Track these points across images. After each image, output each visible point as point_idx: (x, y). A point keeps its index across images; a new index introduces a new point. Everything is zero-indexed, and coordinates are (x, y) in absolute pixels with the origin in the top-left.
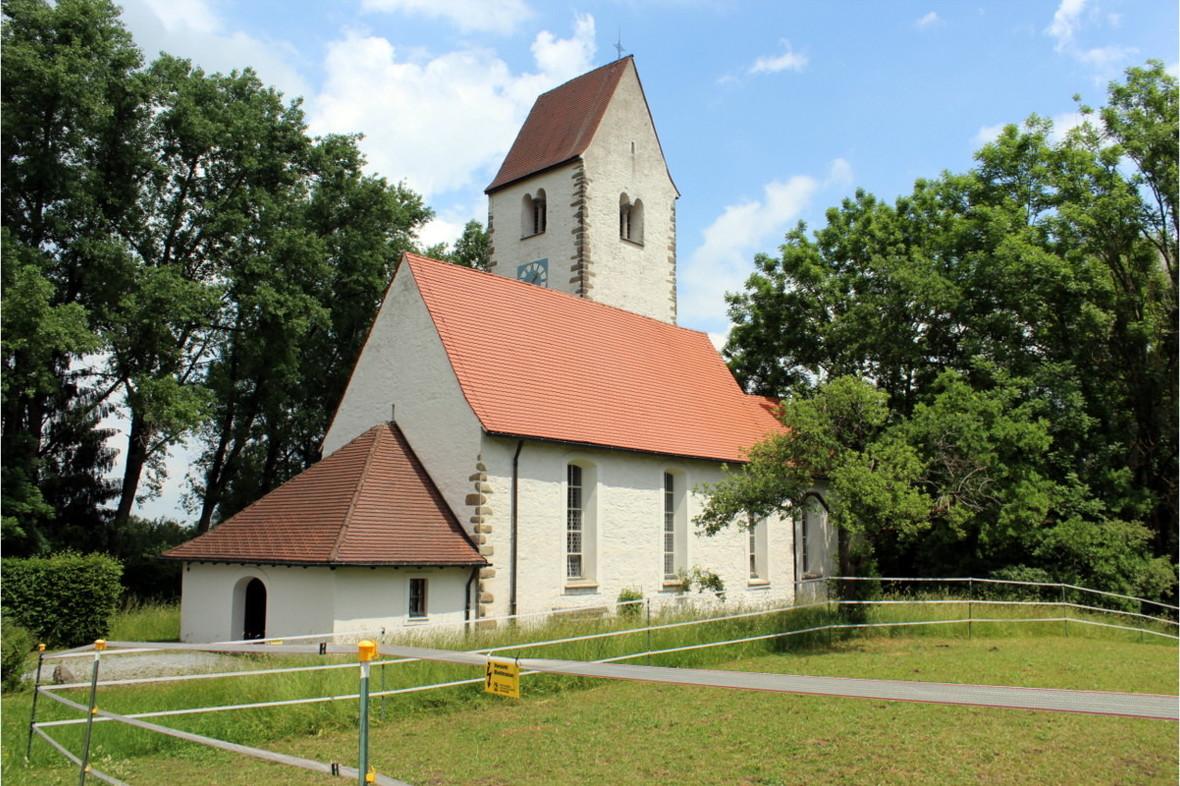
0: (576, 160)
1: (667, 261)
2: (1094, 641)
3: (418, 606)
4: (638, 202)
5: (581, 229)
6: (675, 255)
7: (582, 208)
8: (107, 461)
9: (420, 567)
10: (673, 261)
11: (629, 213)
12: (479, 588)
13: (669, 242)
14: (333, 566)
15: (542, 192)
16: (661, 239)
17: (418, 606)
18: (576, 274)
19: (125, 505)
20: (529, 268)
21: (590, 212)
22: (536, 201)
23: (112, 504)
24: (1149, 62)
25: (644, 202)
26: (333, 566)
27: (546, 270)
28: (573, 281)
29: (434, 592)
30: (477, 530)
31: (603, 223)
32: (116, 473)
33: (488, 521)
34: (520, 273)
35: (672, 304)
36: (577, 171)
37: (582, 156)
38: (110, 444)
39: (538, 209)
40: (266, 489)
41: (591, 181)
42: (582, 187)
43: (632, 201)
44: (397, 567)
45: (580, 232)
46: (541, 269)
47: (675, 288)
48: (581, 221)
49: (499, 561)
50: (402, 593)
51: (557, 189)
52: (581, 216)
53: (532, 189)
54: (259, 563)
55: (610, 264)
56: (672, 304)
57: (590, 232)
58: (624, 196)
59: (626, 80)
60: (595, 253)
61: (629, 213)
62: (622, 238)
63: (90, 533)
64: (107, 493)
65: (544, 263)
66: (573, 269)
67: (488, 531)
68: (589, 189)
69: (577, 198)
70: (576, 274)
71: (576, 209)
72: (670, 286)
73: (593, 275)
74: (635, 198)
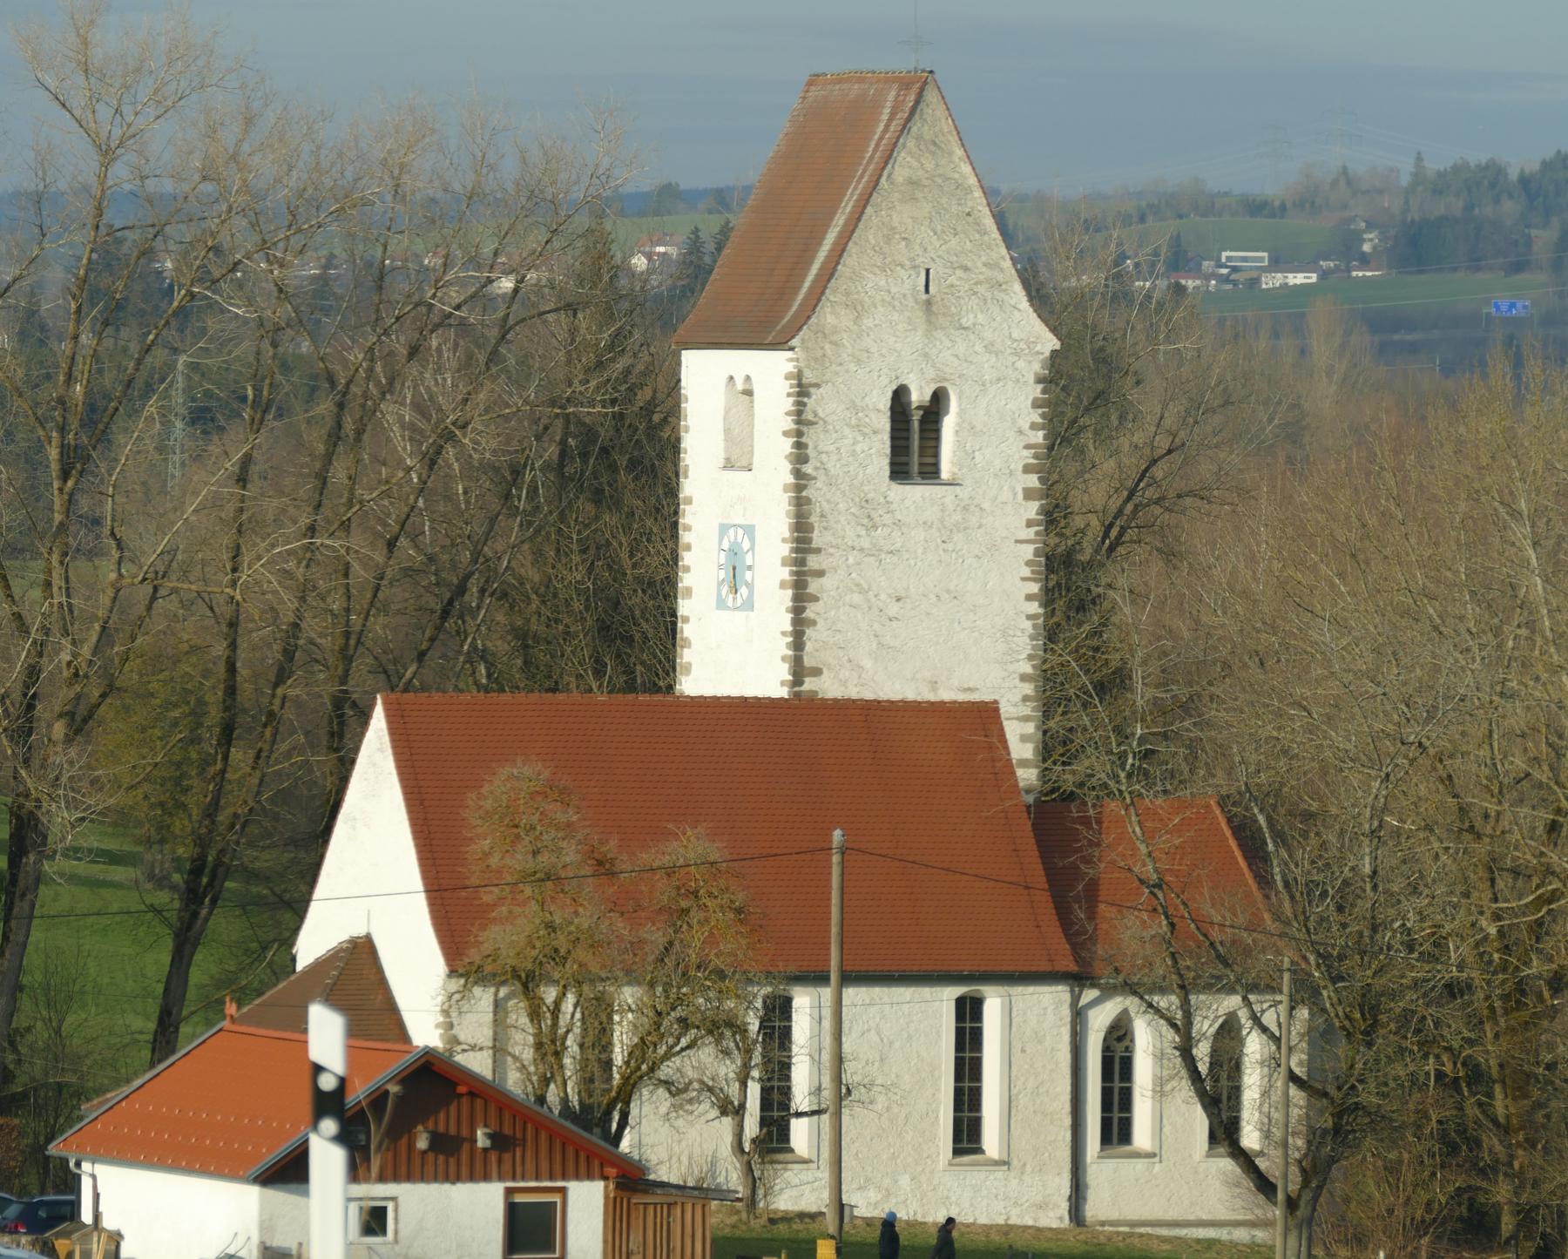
65: (749, 530)
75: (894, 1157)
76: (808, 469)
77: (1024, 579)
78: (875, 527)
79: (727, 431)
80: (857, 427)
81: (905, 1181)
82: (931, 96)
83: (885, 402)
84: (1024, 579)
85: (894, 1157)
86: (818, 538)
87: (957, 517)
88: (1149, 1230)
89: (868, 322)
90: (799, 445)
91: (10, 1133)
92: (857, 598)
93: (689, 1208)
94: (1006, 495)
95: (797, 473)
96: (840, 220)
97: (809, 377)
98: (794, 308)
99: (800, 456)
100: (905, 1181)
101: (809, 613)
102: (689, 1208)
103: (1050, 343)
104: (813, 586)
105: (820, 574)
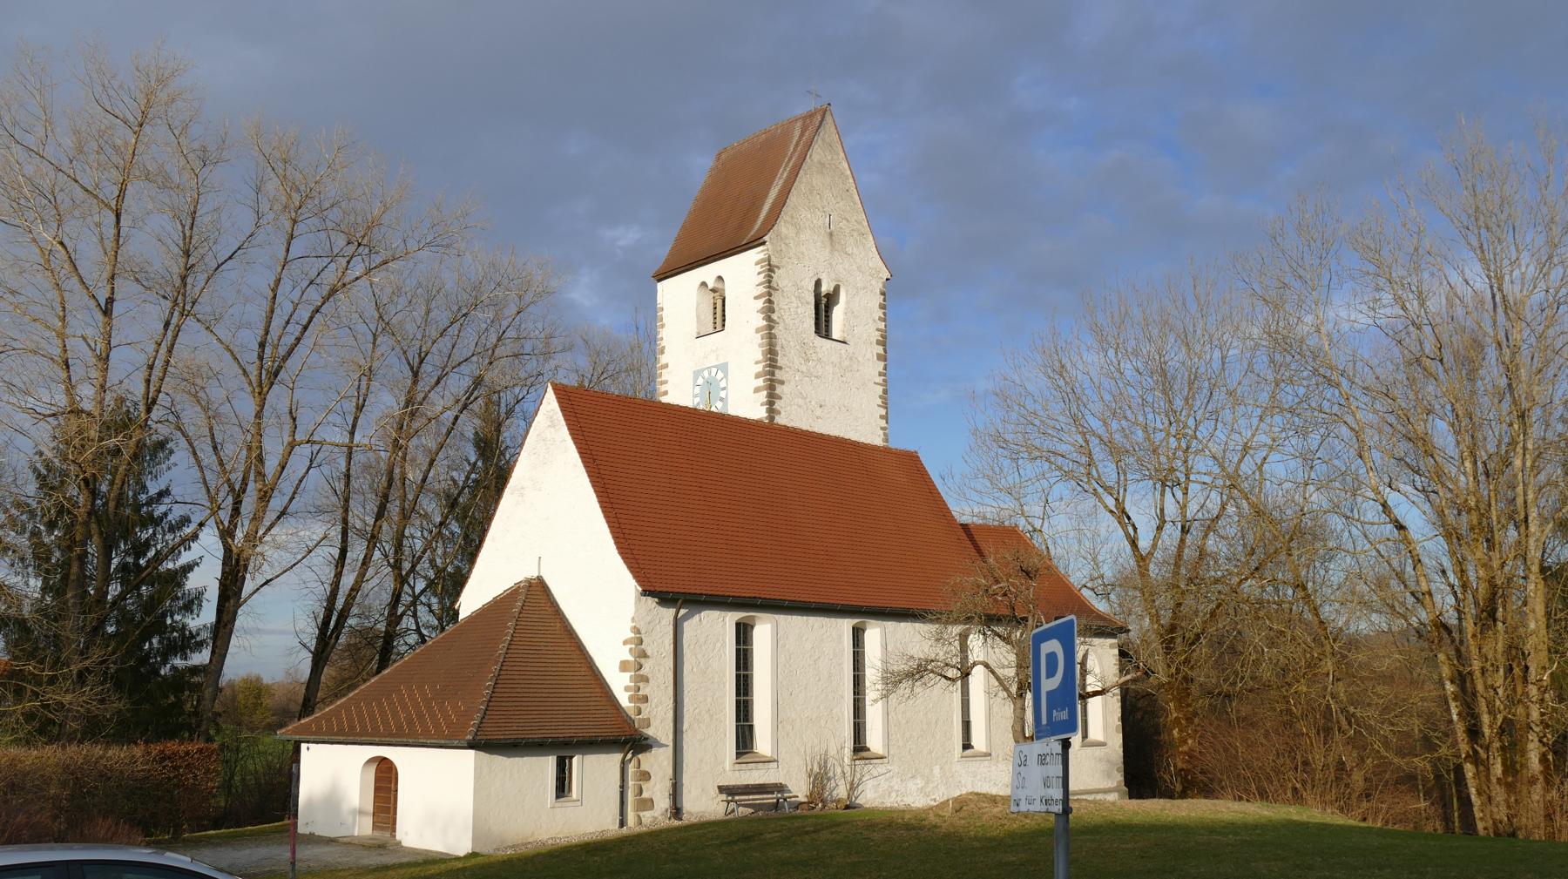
2: (1425, 288)
8: (192, 604)
11: (824, 306)
19: (220, 653)
20: (706, 373)
23: (202, 657)
27: (726, 376)
32: (207, 616)
34: (695, 379)
35: (883, 412)
38: (193, 582)
40: (501, 478)
46: (721, 374)
55: (804, 368)
56: (883, 412)
61: (824, 306)
62: (818, 331)
64: (188, 642)
65: (723, 367)
69: (762, 290)
73: (782, 383)
75: (930, 752)
76: (774, 317)
77: (818, 283)
78: (808, 360)
79: (698, 317)
80: (798, 298)
81: (936, 770)
82: (828, 118)
83: (812, 287)
84: (818, 283)
85: (930, 752)
86: (781, 361)
87: (847, 363)
88: (1099, 797)
89: (803, 237)
90: (770, 301)
91: (209, 757)
92: (801, 401)
93: (380, 705)
94: (869, 355)
95: (769, 319)
96: (773, 193)
97: (774, 261)
98: (757, 227)
99: (769, 310)
100: (936, 770)
101: (776, 406)
102: (380, 705)
103: (886, 275)
104: (779, 390)
105: (782, 383)
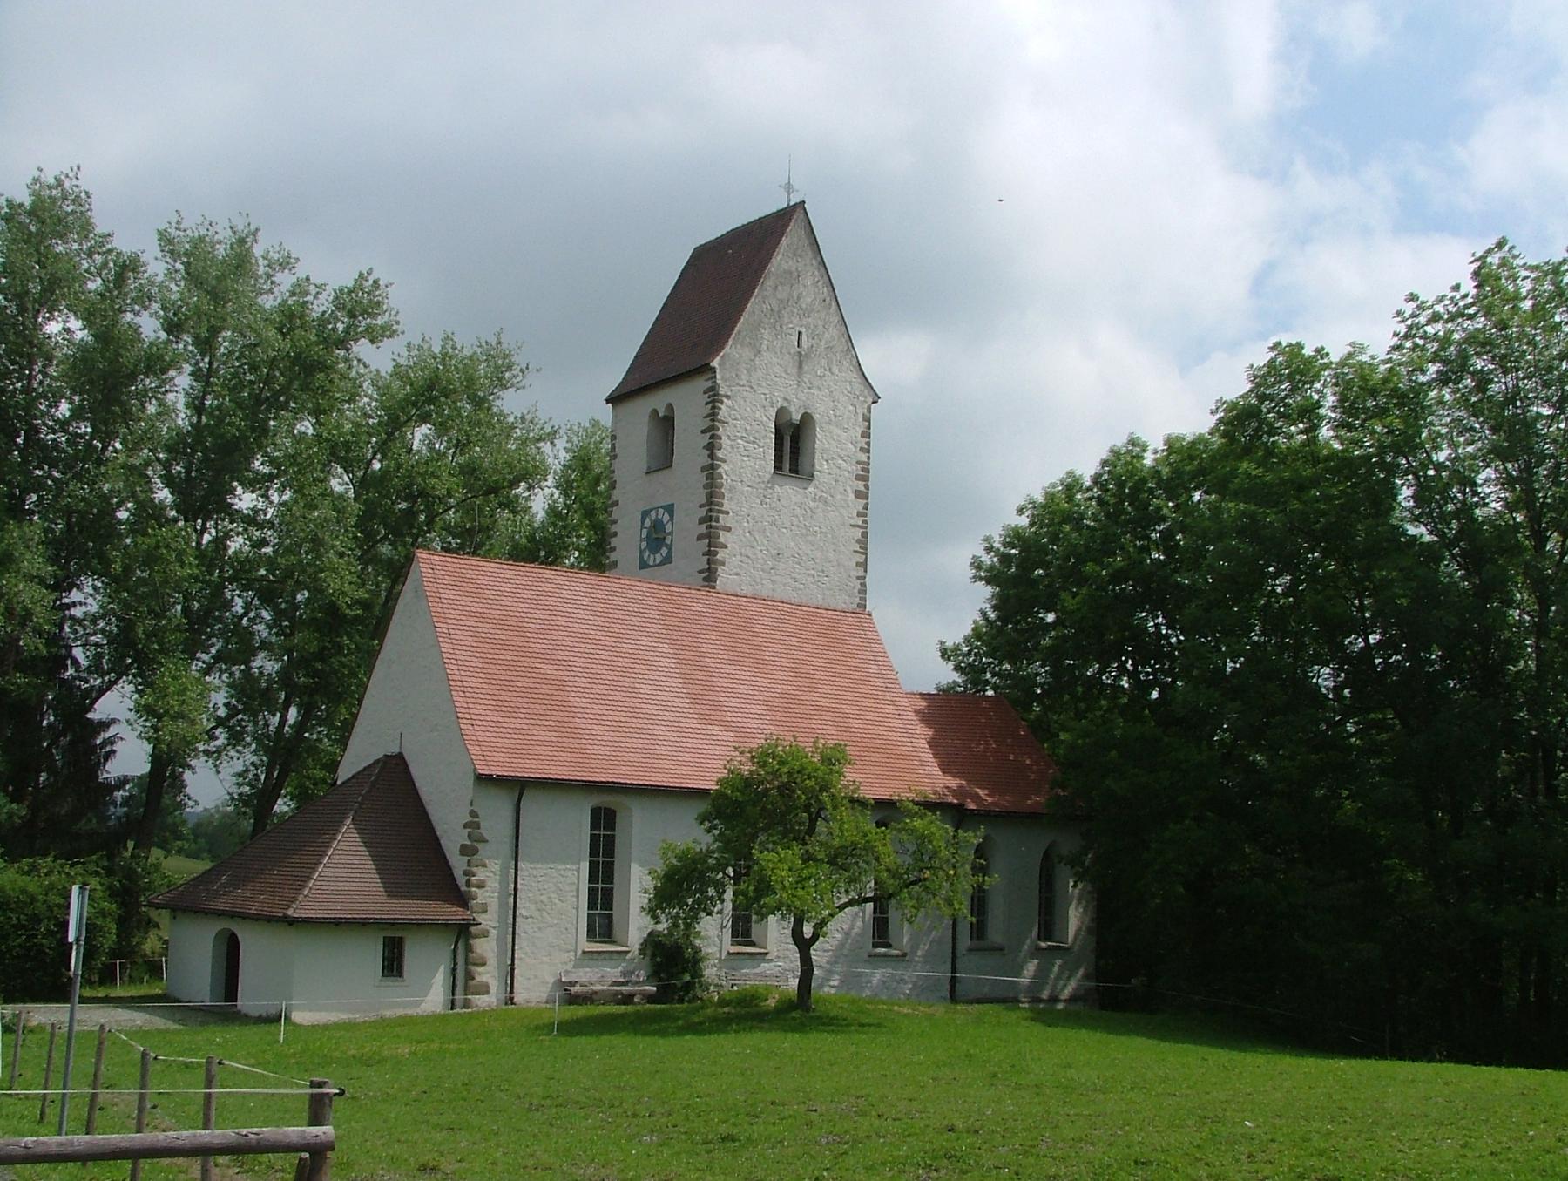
0: (705, 369)
1: (852, 496)
3: (393, 965)
4: (807, 418)
5: (712, 467)
6: (867, 487)
7: (712, 437)
9: (393, 924)
10: (862, 495)
12: (469, 949)
13: (857, 470)
14: (292, 922)
15: (670, 407)
16: (844, 465)
17: (393, 965)
18: (703, 529)
21: (725, 441)
22: (665, 417)
24: (1021, 511)
25: (816, 416)
26: (292, 922)
28: (699, 538)
29: (412, 956)
30: (468, 883)
31: (747, 453)
33: (481, 875)
36: (709, 384)
37: (715, 364)
39: (665, 424)
41: (728, 397)
42: (714, 407)
43: (796, 417)
44: (363, 924)
45: (711, 471)
46: (666, 518)
47: (865, 535)
48: (712, 456)
49: (488, 921)
50: (371, 954)
51: (686, 400)
52: (711, 448)
53: (657, 401)
54: (232, 915)
57: (724, 469)
58: (781, 412)
59: (792, 238)
60: (731, 499)
63: (248, 739)
65: (670, 509)
66: (701, 521)
67: (481, 885)
68: (723, 412)
70: (703, 529)
71: (706, 439)
72: (858, 533)
74: (802, 411)
